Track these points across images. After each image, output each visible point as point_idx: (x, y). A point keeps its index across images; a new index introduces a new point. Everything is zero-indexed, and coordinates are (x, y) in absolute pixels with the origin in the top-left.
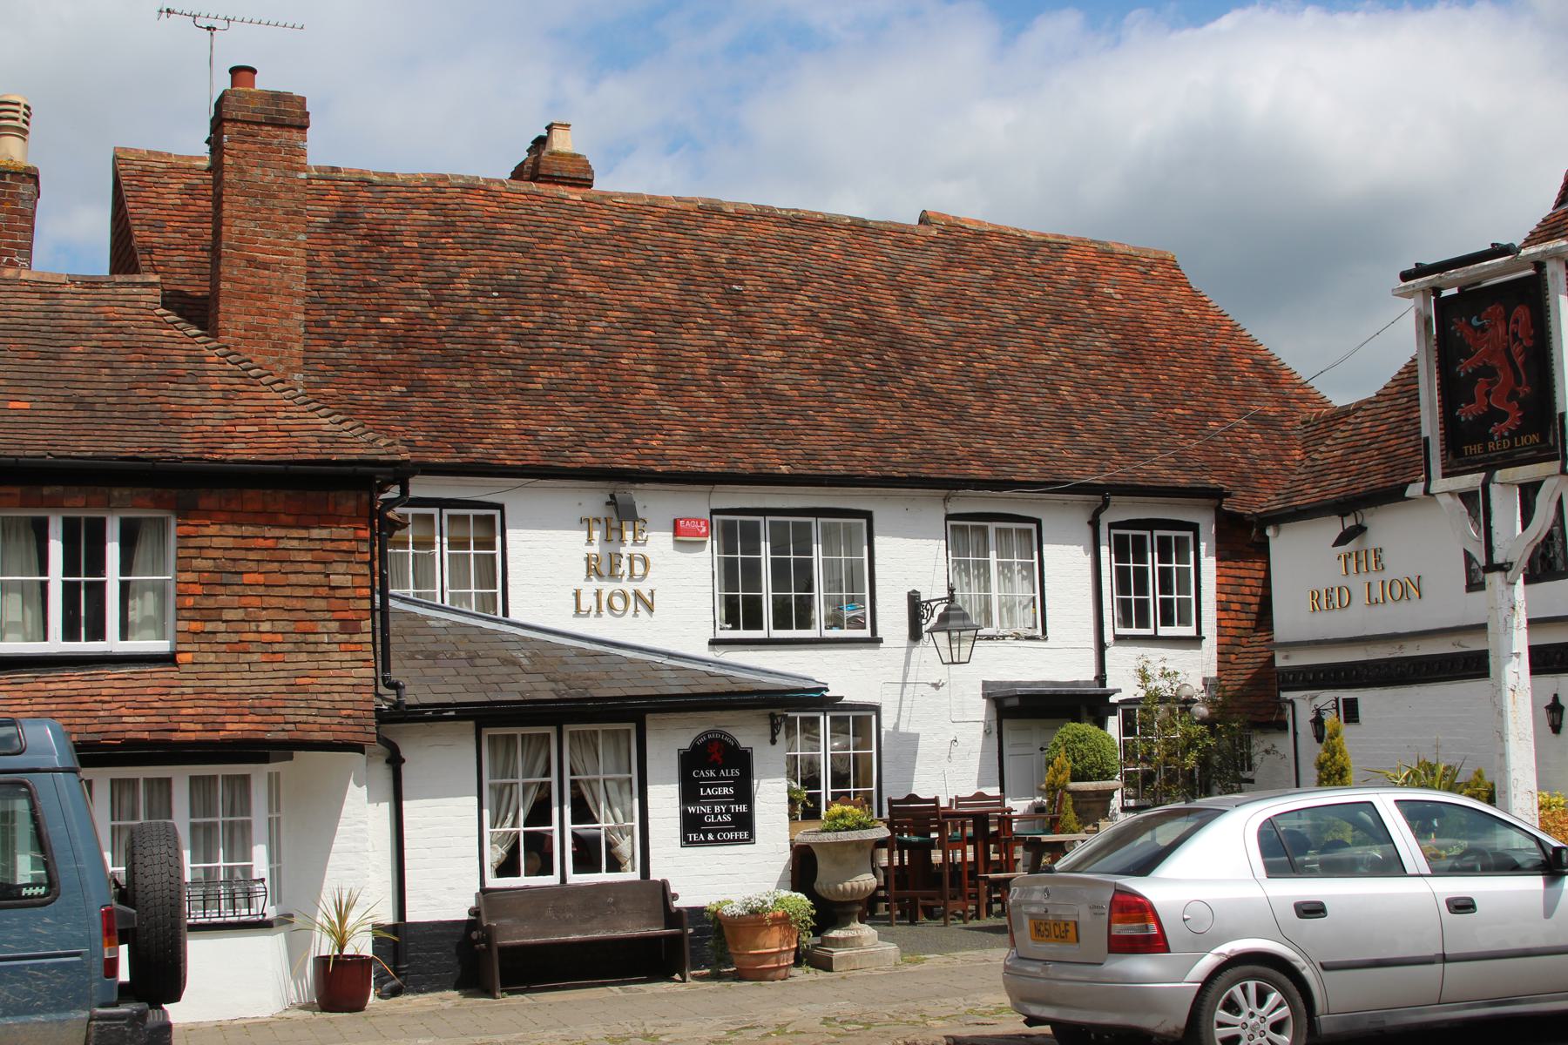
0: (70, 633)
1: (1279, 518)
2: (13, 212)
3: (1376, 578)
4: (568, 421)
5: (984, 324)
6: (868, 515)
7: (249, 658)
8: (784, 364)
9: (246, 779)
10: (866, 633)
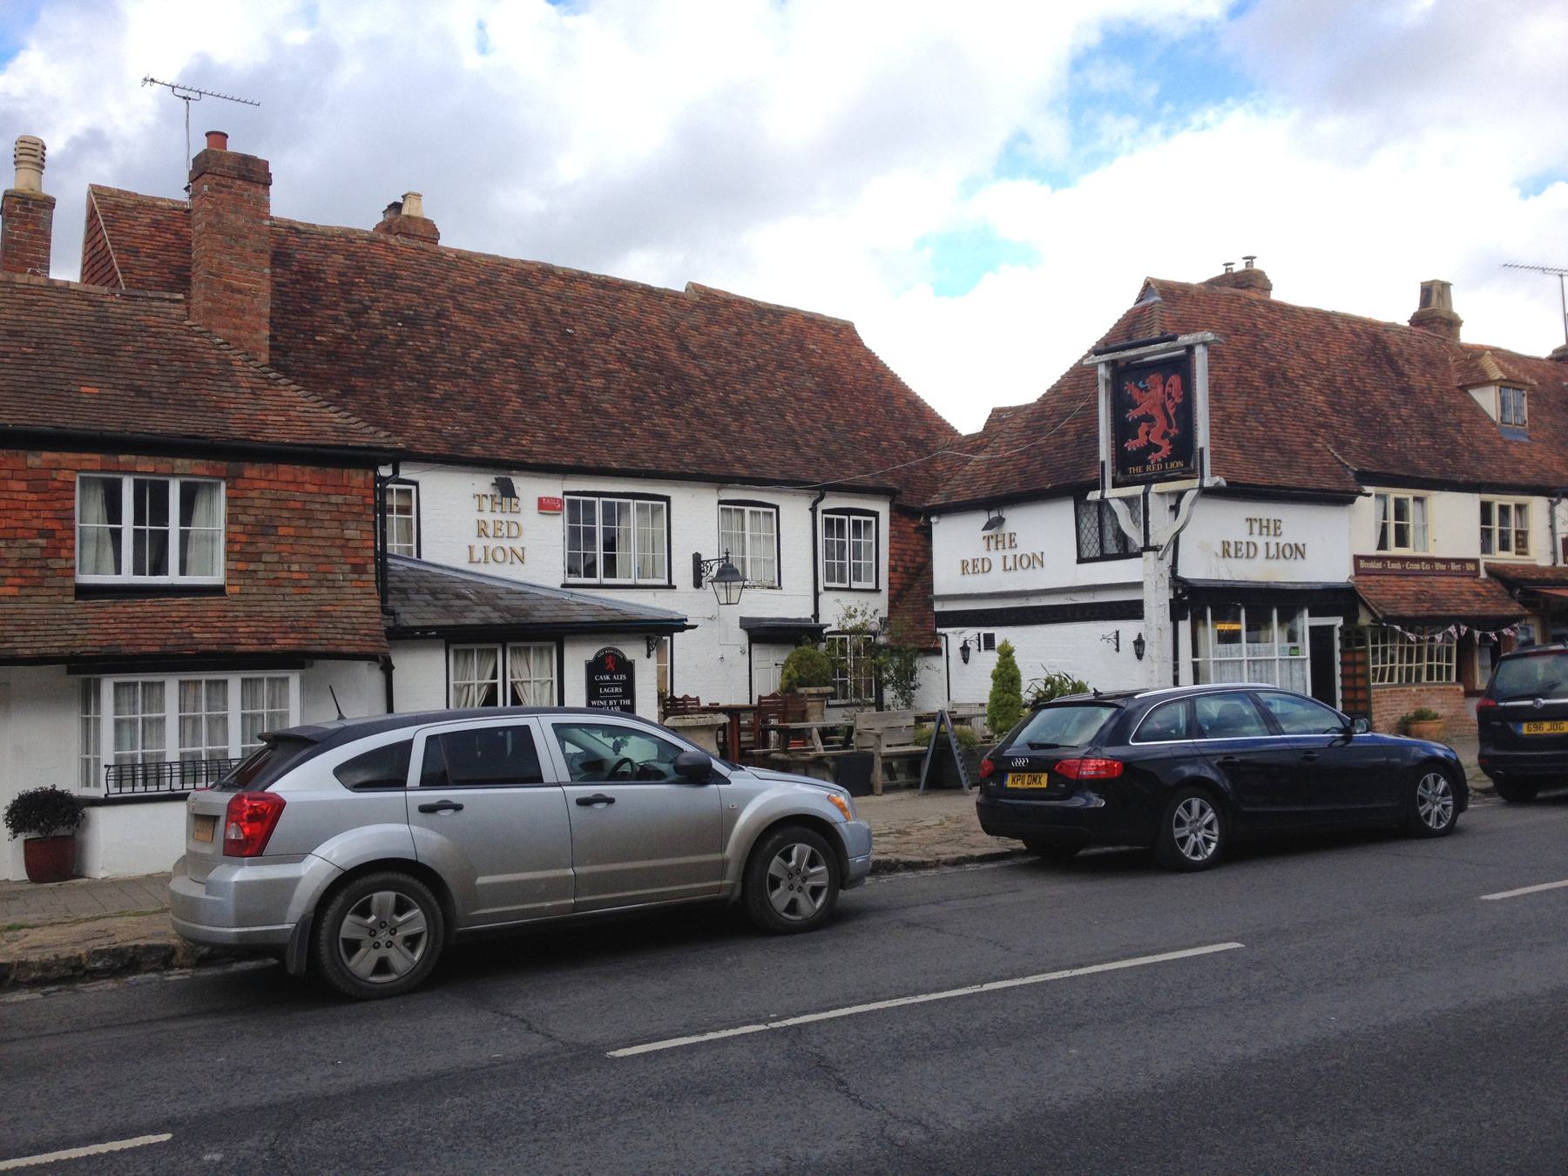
0: (138, 570)
1: (946, 510)
2: (36, 232)
3: (1010, 553)
4: (461, 423)
5: (735, 367)
6: (667, 499)
7: (283, 590)
8: (606, 389)
9: (225, 682)
10: (665, 582)
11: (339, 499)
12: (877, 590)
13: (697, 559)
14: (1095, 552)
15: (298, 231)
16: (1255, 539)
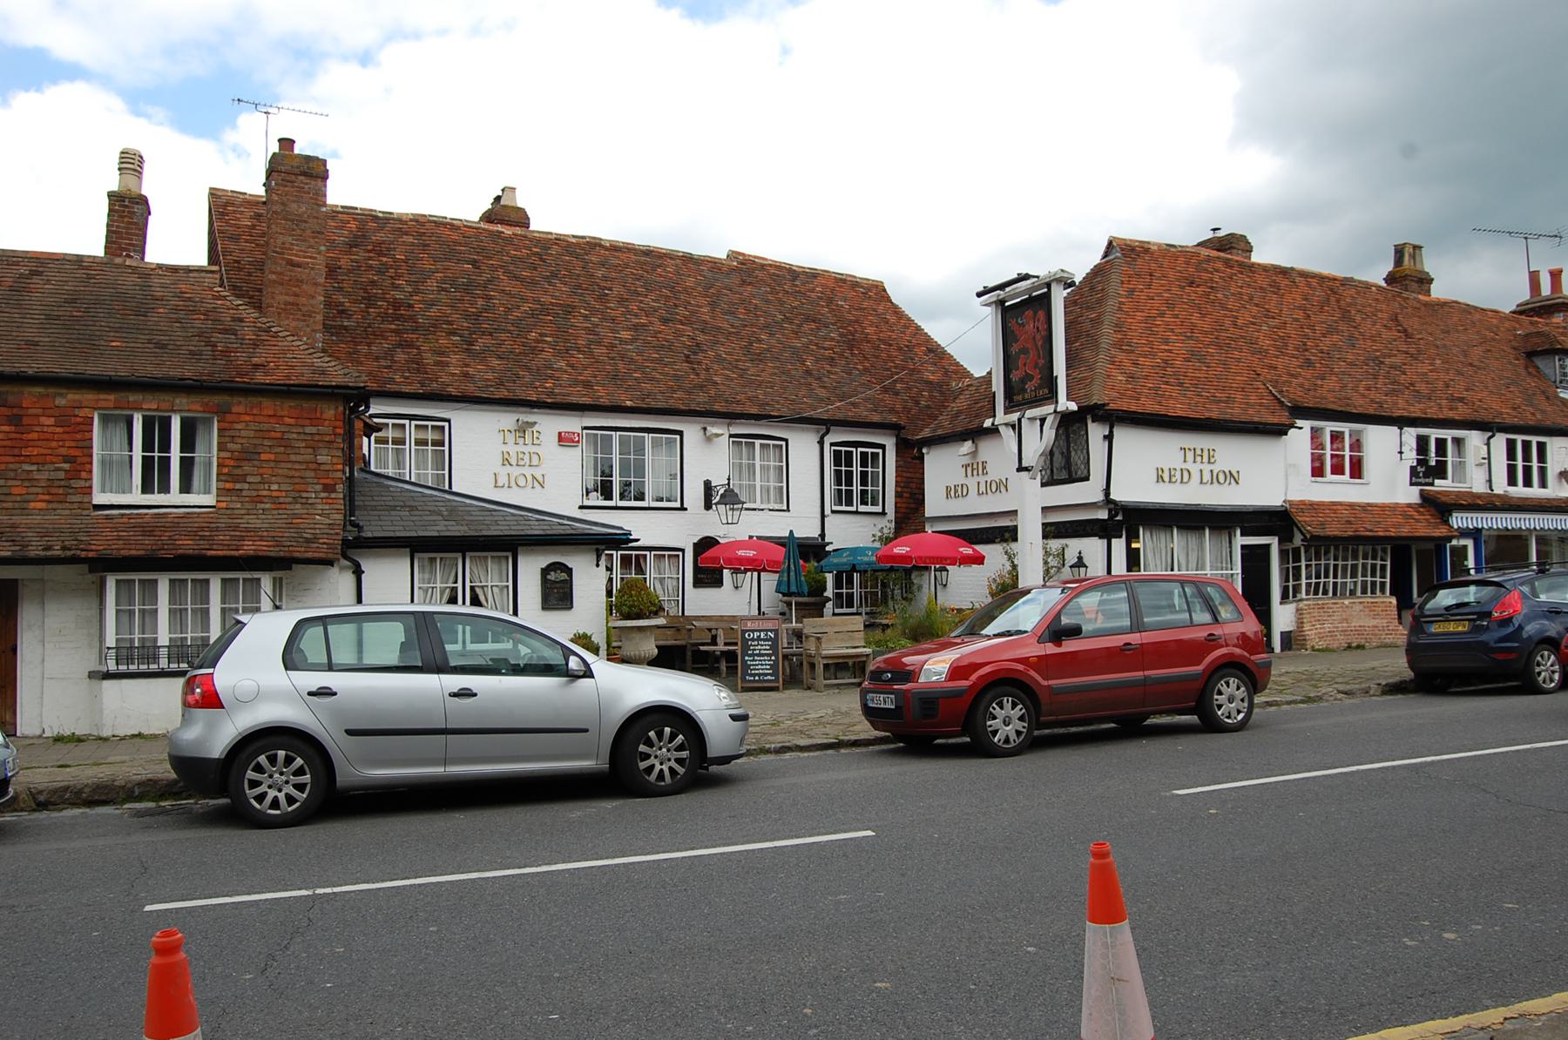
3: (982, 479)
4: (493, 370)
6: (681, 433)
9: (207, 581)
10: (678, 505)
11: (313, 430)
12: (883, 513)
13: (707, 484)
14: (1064, 475)
15: (376, 217)
16: (1190, 465)
